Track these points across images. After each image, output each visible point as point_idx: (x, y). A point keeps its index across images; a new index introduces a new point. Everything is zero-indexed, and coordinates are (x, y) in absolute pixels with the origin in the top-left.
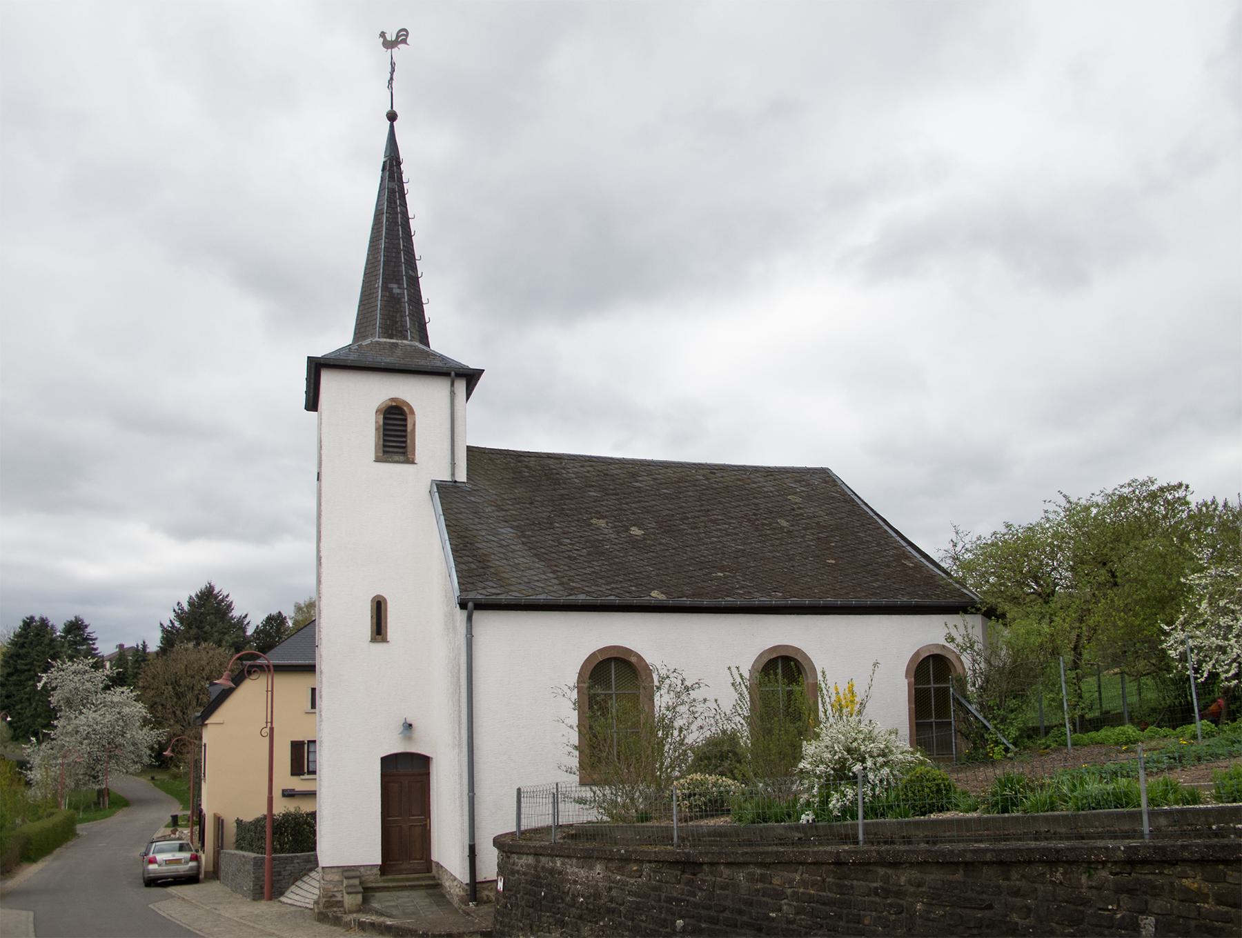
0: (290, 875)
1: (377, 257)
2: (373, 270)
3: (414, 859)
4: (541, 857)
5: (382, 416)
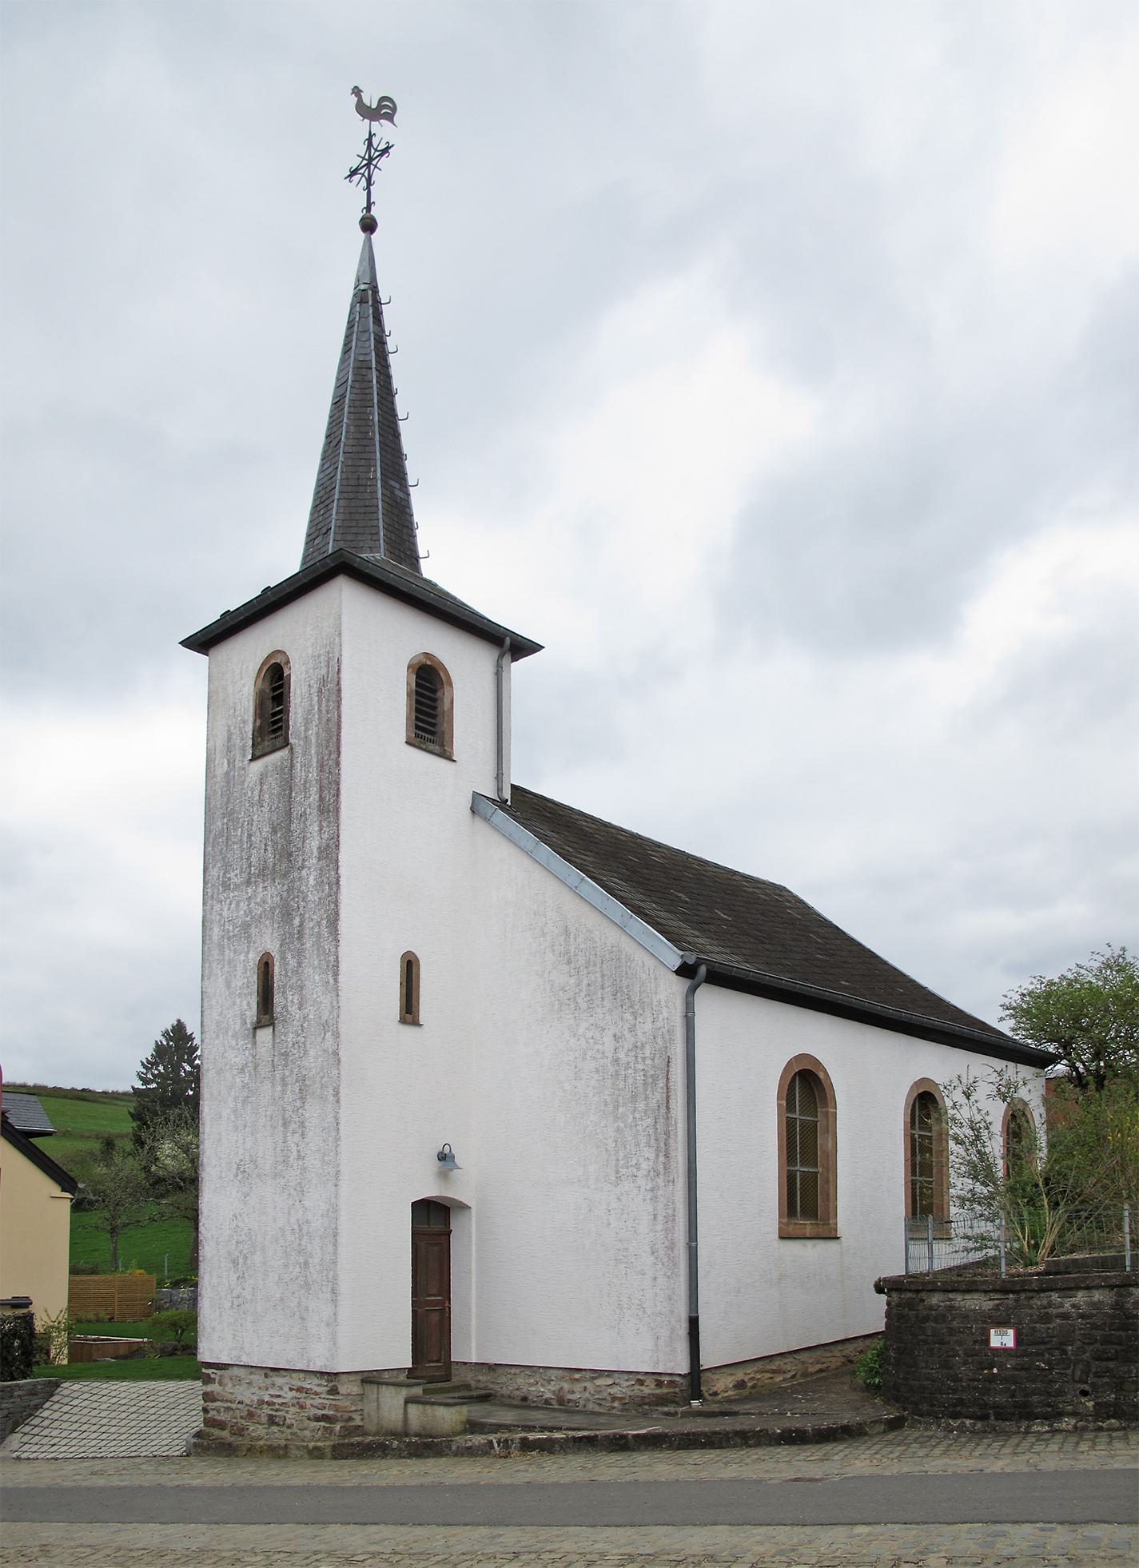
0: (7, 1416)
1: (367, 433)
2: (360, 449)
3: (429, 1362)
4: (1131, 1289)
5: (415, 676)
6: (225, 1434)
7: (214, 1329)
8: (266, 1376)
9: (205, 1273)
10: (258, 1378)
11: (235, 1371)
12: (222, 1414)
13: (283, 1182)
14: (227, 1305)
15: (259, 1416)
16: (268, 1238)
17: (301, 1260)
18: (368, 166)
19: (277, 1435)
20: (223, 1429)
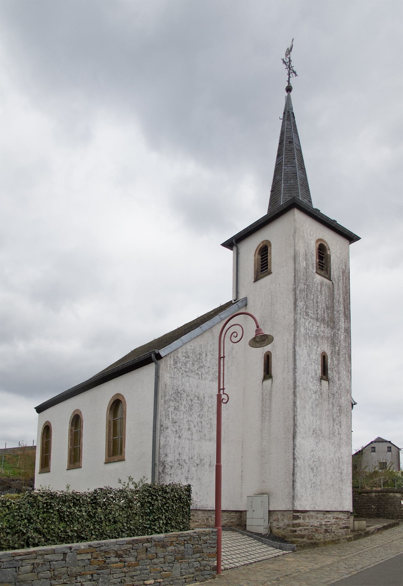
6: (305, 540)
7: (302, 496)
8: (324, 514)
9: (297, 472)
10: (320, 515)
11: (311, 513)
12: (303, 532)
13: (332, 441)
14: (309, 486)
15: (320, 530)
16: (327, 461)
17: (340, 471)
18: (290, 69)
19: (329, 537)
20: (303, 538)
